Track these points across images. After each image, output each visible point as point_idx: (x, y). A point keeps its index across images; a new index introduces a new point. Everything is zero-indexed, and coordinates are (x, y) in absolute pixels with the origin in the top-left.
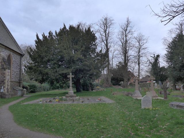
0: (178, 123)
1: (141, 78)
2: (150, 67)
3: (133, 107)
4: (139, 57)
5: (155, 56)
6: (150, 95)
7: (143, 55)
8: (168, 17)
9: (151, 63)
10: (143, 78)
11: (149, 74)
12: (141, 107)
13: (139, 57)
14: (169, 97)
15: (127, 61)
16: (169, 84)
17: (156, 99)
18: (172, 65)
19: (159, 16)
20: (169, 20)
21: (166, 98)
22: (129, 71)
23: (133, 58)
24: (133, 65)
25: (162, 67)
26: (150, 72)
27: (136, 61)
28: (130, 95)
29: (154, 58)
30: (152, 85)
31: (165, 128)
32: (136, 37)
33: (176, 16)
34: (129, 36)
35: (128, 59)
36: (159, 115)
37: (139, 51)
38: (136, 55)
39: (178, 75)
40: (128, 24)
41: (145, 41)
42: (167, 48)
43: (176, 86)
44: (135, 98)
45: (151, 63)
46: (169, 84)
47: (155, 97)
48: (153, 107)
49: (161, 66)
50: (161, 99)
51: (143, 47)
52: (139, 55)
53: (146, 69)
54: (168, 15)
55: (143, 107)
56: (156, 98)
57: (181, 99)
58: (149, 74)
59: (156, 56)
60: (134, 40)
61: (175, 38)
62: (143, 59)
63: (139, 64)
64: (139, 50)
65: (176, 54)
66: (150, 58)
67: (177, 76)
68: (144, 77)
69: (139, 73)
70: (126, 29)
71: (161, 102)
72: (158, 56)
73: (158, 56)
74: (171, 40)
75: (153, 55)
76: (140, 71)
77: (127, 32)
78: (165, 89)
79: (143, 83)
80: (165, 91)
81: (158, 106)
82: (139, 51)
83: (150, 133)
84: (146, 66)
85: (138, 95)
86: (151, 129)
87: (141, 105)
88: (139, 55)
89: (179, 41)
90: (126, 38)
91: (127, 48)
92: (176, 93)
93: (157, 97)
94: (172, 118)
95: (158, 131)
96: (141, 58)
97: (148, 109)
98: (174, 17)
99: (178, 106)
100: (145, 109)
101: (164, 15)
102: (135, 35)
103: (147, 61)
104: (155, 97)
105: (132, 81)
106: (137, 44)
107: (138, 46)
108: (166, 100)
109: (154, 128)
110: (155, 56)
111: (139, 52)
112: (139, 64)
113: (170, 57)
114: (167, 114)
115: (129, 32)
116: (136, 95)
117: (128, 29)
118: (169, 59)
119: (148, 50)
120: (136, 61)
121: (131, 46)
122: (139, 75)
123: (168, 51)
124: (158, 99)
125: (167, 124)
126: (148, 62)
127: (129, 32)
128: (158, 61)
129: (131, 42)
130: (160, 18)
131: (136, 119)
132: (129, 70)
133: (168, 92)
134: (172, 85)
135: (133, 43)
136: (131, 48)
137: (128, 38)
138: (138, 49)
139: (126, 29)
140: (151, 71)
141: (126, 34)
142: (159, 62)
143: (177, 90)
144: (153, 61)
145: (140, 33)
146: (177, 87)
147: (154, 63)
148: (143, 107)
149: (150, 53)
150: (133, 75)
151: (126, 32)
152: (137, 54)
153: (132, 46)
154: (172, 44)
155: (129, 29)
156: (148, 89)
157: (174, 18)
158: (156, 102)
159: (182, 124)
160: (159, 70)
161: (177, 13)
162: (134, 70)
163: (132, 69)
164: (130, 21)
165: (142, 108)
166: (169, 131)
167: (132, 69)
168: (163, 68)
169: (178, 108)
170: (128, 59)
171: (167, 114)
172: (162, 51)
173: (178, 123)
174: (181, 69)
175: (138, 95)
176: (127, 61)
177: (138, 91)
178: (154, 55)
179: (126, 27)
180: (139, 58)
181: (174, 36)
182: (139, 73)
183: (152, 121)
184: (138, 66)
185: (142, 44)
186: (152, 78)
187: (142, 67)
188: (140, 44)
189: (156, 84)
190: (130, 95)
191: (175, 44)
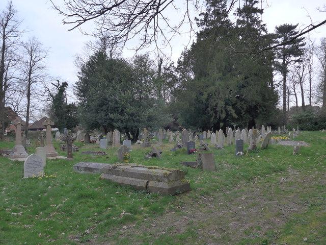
0: (81, 196)
1: (30, 122)
2: (49, 102)
3: (8, 176)
4: (29, 81)
5: (59, 84)
6: (43, 153)
7: (37, 80)
8: (76, 18)
9: (52, 96)
10: (36, 122)
11: (47, 116)
12: (23, 177)
13: (29, 81)
14: (76, 155)
15: (4, 87)
16: (79, 134)
17: (53, 160)
18: (85, 101)
19: (61, 12)
20: (77, 23)
21: (70, 156)
22: (9, 108)
23: (17, 84)
24: (17, 96)
25: (70, 105)
26: (50, 112)
27: (24, 89)
28: (5, 155)
29: (58, 87)
30: (49, 135)
31: (60, 207)
32: (25, 42)
33: (89, 19)
34: (11, 39)
35: (5, 83)
36: (53, 186)
37: (30, 71)
38: (24, 78)
39: (94, 119)
40: (10, 13)
41: (42, 55)
42: (79, 73)
43: (89, 136)
44: (14, 160)
45: (52, 96)
46: (79, 134)
47: (52, 155)
48: (46, 173)
49: (69, 103)
50: (62, 160)
51: (37, 65)
52: (30, 79)
53: (42, 105)
54: (77, 14)
55: (26, 176)
56: (54, 158)
57: (93, 157)
58: (47, 116)
59: (61, 84)
60: (22, 48)
61: (94, 58)
62: (37, 87)
63: (29, 95)
64: (31, 70)
65: (93, 84)
66: (51, 87)
67: (92, 120)
68: (38, 119)
69: (28, 112)
70: (5, 22)
71: (63, 164)
72: (65, 84)
73: (65, 84)
74: (86, 59)
75: (56, 83)
76: (31, 109)
77: (6, 30)
78: (69, 141)
79: (33, 132)
80: (70, 146)
81: (55, 171)
82: (30, 71)
83: (32, 221)
84: (42, 101)
85: (21, 154)
86: (36, 213)
87: (23, 172)
88: (30, 79)
89: (98, 64)
90: (4, 42)
91: (6, 63)
92: (88, 147)
93: (55, 155)
94: (74, 188)
95: (48, 215)
96: (33, 85)
97: (36, 178)
98: (85, 20)
99: (86, 169)
100: (29, 178)
101: (69, 12)
102: (25, 38)
103: (44, 91)
104: (52, 155)
105: (12, 127)
106: (27, 58)
107: (29, 61)
108: (69, 159)
109: (41, 210)
110: (59, 84)
111: (30, 73)
112: (29, 95)
113: (84, 89)
114: (67, 183)
115: (12, 30)
116: (16, 154)
117: (9, 24)
118: (81, 91)
119: (48, 72)
120: (24, 89)
121: (15, 60)
122: (27, 117)
123: (81, 78)
124: (57, 159)
125: (64, 200)
126: (46, 94)
127: (12, 30)
128: (64, 93)
129: (15, 52)
130: (64, 17)
131: (10, 198)
132: (8, 106)
133: (74, 147)
134: (85, 134)
135: (18, 54)
136: (13, 62)
137: (7, 42)
138: (29, 67)
139: (7, 24)
140: (52, 110)
141: (4, 33)
142: (66, 95)
143: (90, 142)
144: (55, 92)
145: (34, 38)
146: (92, 138)
147: (57, 96)
148: (26, 176)
149: (50, 77)
150: (15, 115)
151: (4, 29)
152: (26, 75)
153: (16, 58)
154: (88, 67)
155: (10, 23)
156: (42, 142)
157: (85, 22)
158: (52, 165)
159: (2, 229)
160: (65, 110)
161: (91, 14)
162: (19, 106)
163: (15, 104)
164: (16, 9)
165: (25, 177)
166: (67, 211)
167: (15, 104)
168: (72, 106)
169: (87, 172)
170: (5, 83)
171: (67, 183)
172: (72, 76)
173: (81, 196)
174: (98, 110)
175: (21, 154)
176: (4, 87)
177: (21, 146)
178: (58, 81)
179: (6, 19)
180: (30, 84)
181: (92, 53)
182: (28, 112)
183: (39, 199)
184: (26, 99)
185: (37, 59)
186: (49, 123)
187: (33, 101)
188: (33, 58)
189: (58, 134)
190: (5, 155)
191: (91, 66)
